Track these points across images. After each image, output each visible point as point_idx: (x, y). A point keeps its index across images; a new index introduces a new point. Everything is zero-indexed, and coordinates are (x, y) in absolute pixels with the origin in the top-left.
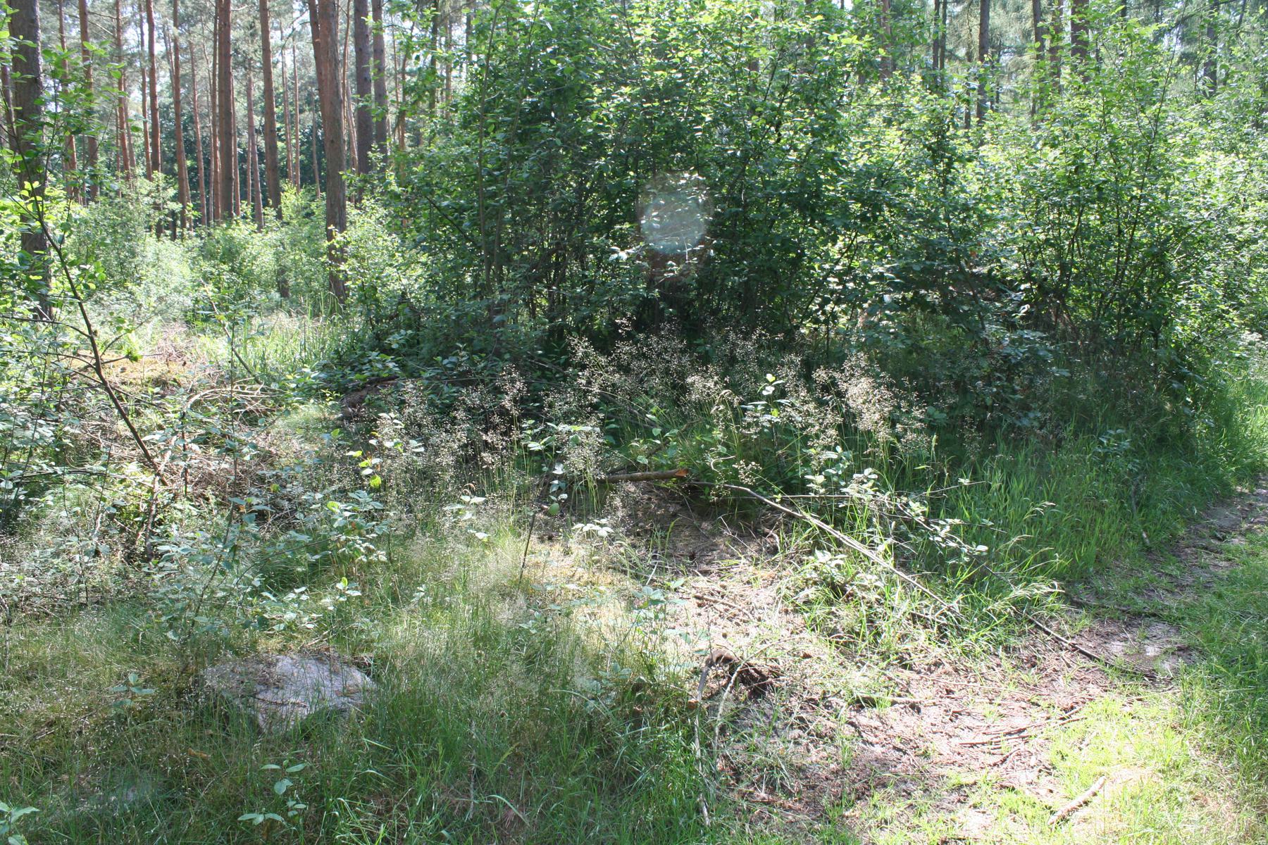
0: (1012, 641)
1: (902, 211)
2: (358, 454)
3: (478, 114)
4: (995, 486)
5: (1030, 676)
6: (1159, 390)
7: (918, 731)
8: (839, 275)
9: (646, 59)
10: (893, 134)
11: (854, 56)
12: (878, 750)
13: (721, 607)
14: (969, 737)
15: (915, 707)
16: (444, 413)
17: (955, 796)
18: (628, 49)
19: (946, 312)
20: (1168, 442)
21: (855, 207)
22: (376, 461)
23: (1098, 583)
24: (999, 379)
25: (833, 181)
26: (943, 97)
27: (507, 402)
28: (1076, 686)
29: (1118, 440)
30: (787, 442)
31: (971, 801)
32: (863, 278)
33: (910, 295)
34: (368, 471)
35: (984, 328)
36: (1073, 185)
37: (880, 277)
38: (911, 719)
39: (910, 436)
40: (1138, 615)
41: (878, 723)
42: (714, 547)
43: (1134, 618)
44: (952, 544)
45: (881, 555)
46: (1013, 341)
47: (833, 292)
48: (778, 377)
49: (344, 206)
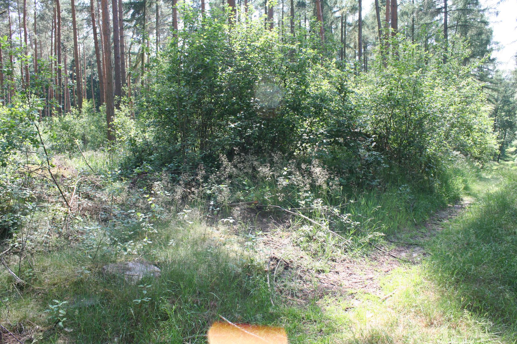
0: (369, 252)
1: (330, 110)
2: (148, 196)
3: (174, 75)
4: (363, 203)
5: (375, 263)
6: (422, 172)
7: (338, 279)
8: (307, 133)
9: (239, 58)
10: (326, 82)
11: (312, 56)
12: (326, 285)
13: (272, 245)
14: (355, 281)
15: (337, 273)
16: (175, 181)
17: (350, 296)
18: (230, 52)
19: (345, 145)
20: (424, 189)
21: (312, 109)
22: (153, 199)
23: (398, 236)
24: (365, 168)
25: (304, 99)
26: (342, 71)
27: (198, 178)
28: (389, 265)
29: (406, 189)
30: (291, 191)
31: (355, 298)
32: (316, 134)
33: (332, 140)
34: (150, 202)
35: (359, 151)
36: (389, 100)
37: (322, 134)
38: (336, 276)
39: (334, 187)
40: (411, 244)
41: (325, 277)
42: (268, 227)
43: (409, 246)
44: (348, 222)
45: (325, 226)
46: (369, 155)
47: (305, 139)
48: (288, 169)
49: (114, 109)
